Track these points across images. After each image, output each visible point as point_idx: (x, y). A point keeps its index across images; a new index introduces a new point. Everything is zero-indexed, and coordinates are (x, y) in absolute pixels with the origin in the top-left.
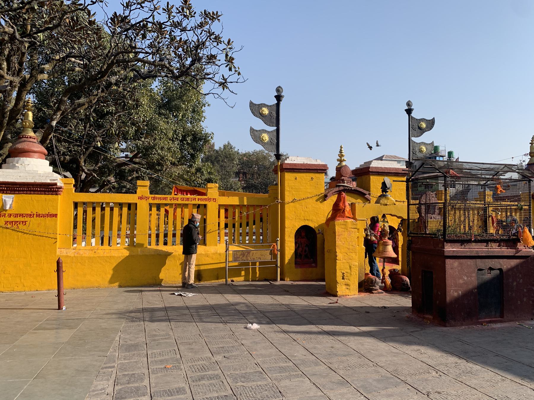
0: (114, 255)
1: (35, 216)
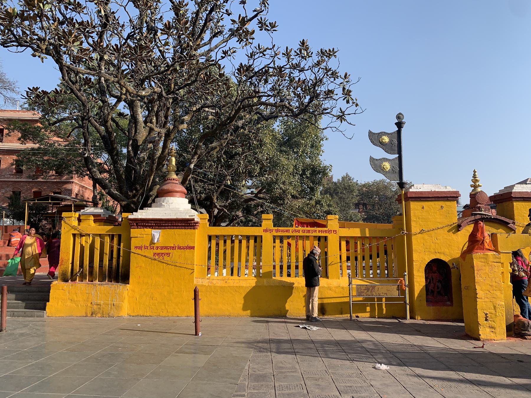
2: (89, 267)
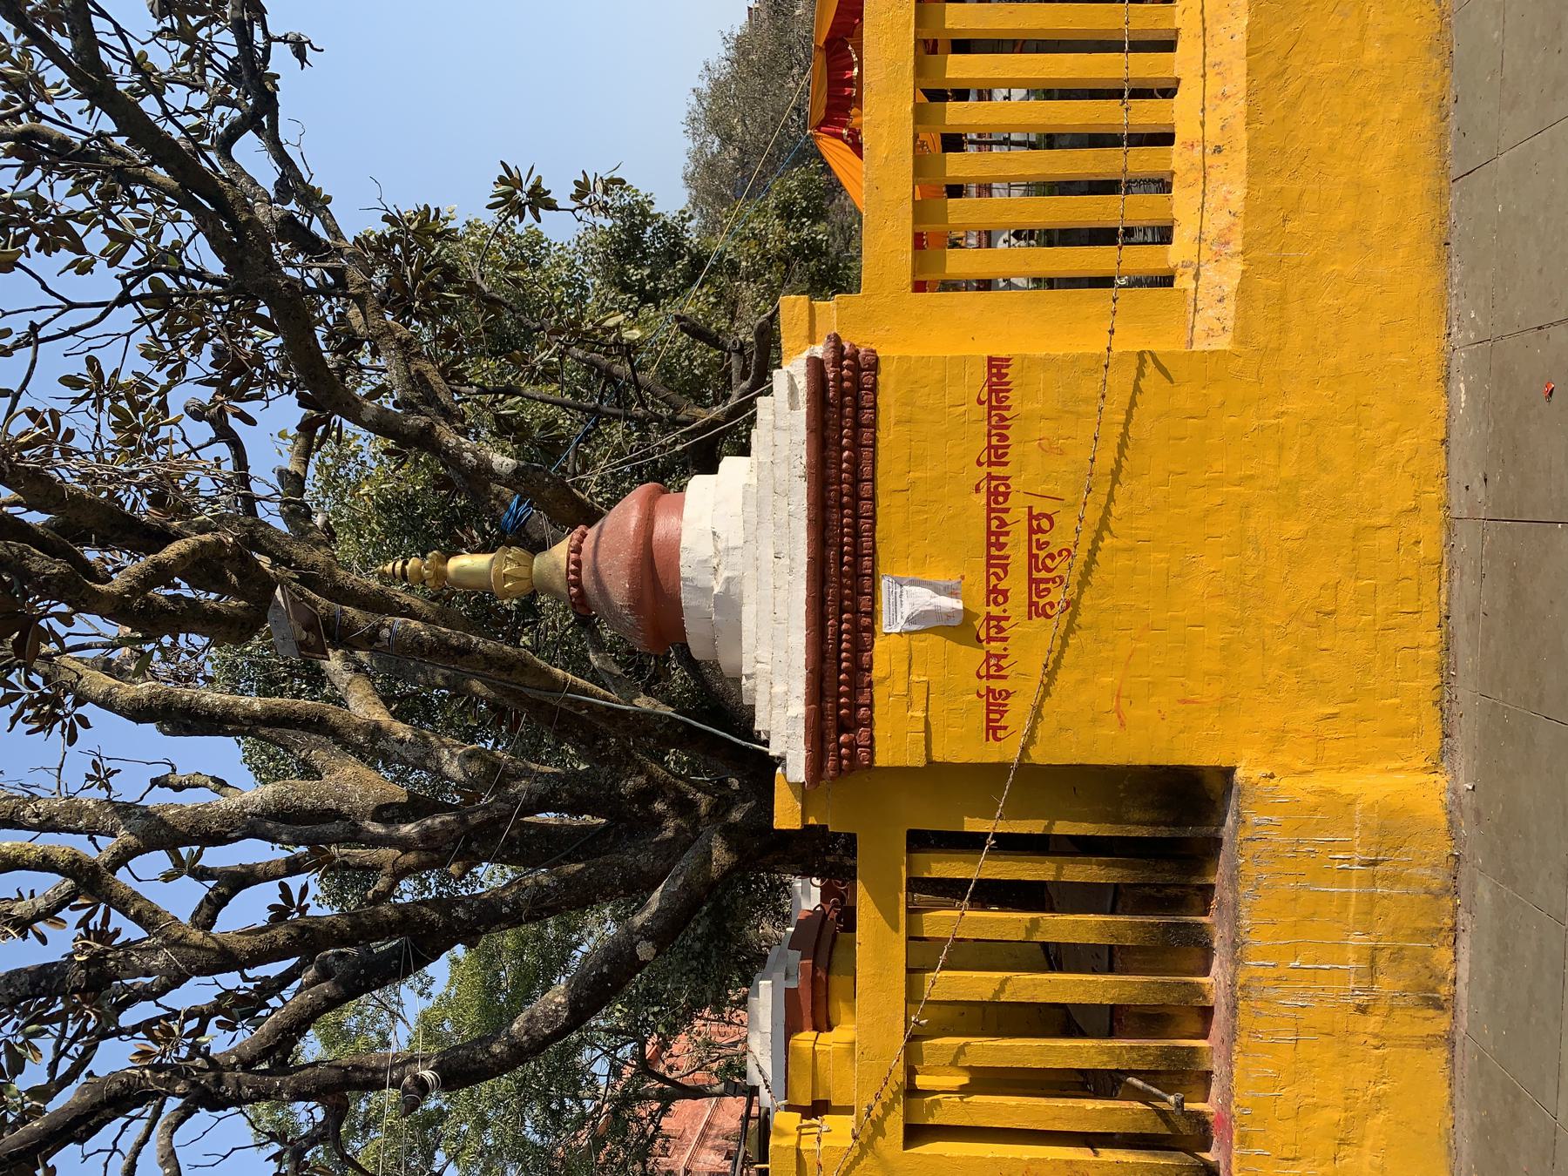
0: (1241, 38)
1: (997, 471)
2: (1111, 1035)
